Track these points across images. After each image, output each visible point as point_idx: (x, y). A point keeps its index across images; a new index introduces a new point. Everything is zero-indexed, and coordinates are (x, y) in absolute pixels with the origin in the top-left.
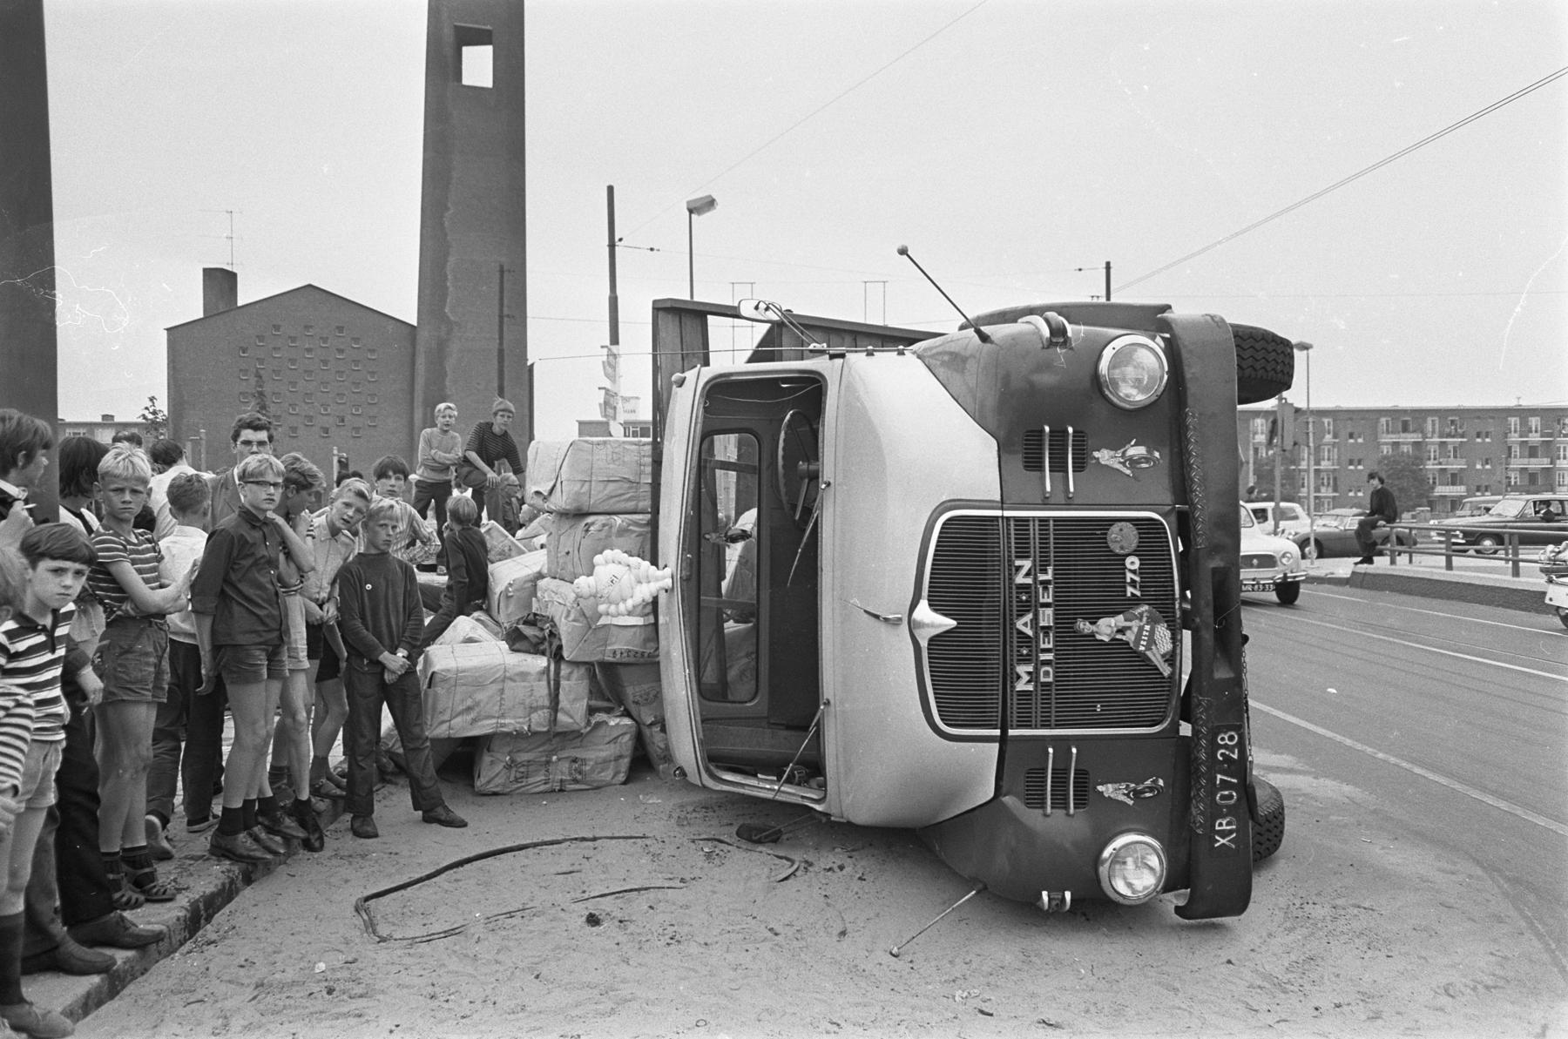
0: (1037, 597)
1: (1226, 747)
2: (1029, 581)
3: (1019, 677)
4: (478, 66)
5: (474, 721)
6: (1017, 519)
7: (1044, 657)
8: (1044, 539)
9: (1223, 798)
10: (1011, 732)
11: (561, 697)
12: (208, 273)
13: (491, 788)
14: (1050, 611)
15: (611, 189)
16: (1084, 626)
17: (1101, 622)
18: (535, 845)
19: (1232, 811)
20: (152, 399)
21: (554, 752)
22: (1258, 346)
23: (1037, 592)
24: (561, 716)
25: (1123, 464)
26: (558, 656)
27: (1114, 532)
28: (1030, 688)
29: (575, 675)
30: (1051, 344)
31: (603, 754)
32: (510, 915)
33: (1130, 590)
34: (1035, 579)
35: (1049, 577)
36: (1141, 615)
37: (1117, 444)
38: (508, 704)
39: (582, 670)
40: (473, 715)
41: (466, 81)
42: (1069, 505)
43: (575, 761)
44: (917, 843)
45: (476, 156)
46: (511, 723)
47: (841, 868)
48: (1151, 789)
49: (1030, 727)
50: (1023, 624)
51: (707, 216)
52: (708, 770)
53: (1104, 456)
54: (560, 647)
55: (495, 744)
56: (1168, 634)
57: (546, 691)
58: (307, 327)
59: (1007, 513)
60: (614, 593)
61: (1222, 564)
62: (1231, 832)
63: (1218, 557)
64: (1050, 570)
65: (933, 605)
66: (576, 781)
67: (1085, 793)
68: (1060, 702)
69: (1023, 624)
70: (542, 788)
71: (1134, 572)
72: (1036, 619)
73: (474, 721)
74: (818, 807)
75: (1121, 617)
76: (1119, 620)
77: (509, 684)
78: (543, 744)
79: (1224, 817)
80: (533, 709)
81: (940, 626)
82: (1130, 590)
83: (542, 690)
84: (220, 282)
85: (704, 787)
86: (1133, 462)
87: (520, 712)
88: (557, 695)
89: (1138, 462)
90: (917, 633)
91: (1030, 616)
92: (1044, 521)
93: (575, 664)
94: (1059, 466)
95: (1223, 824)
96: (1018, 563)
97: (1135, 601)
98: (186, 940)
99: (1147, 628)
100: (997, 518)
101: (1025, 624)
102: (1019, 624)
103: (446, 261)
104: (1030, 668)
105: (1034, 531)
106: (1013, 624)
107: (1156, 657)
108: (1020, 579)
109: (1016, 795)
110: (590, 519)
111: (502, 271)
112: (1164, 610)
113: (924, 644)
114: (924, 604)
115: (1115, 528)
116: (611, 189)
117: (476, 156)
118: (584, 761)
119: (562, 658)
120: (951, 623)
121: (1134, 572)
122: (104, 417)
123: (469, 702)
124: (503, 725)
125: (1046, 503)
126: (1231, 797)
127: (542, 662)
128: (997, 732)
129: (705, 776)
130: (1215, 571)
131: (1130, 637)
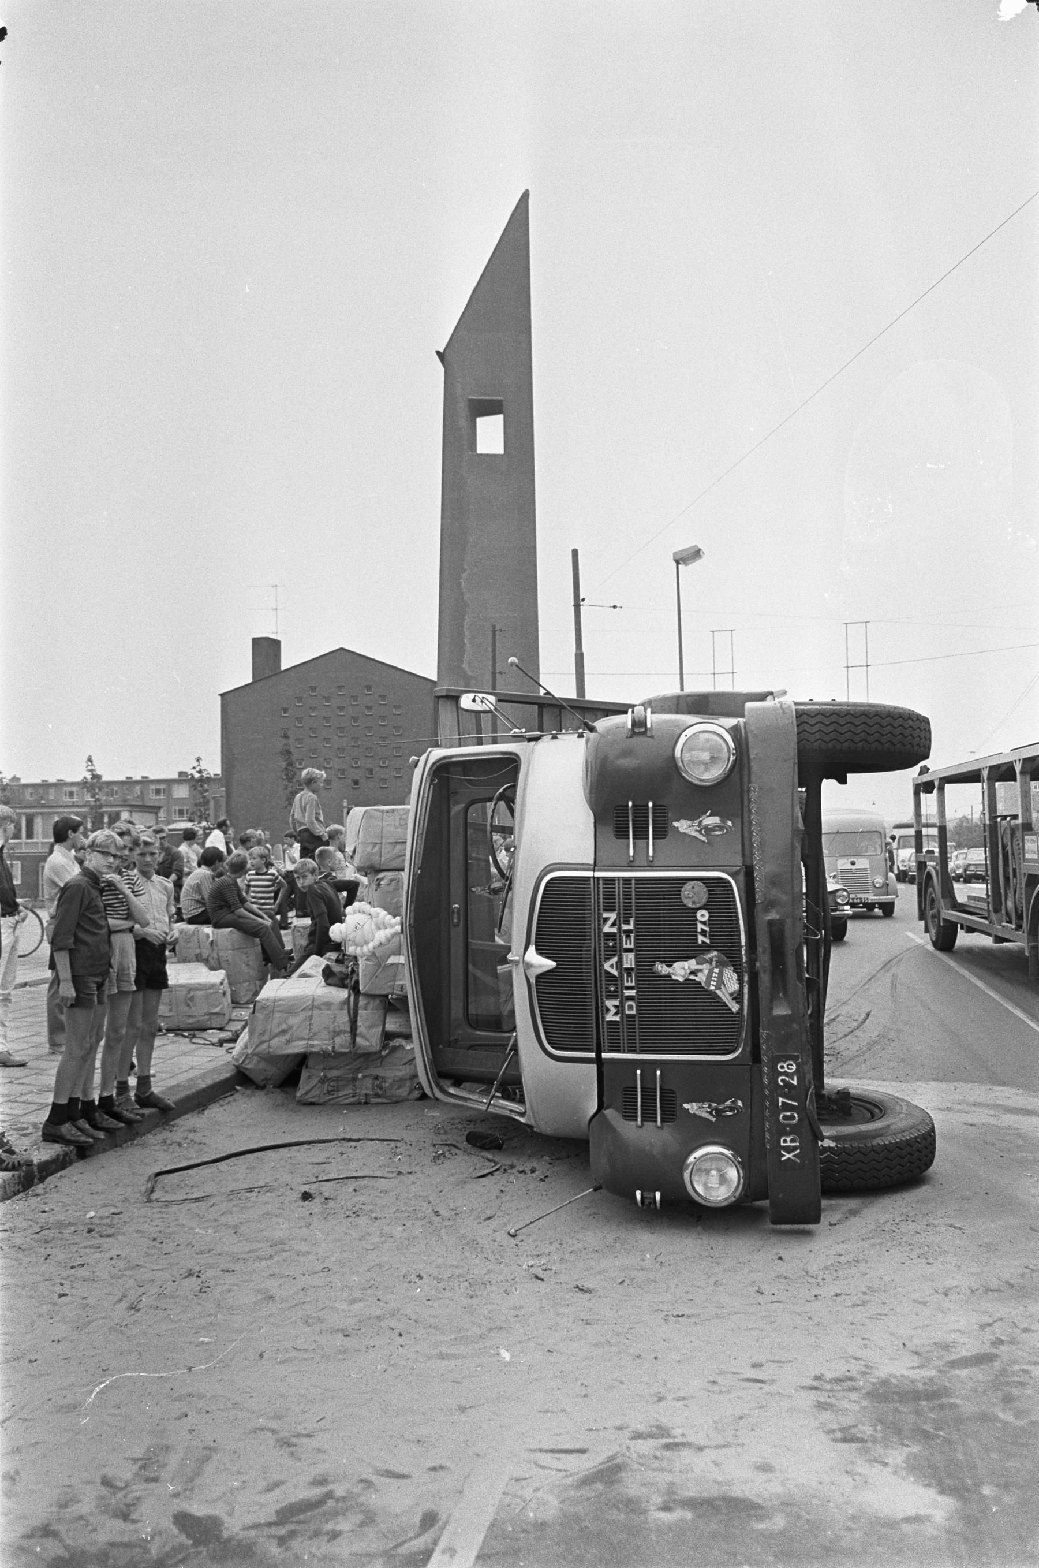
0: (621, 943)
1: (786, 1074)
2: (614, 930)
3: (608, 1010)
4: (490, 435)
5: (288, 1042)
6: (605, 879)
7: (627, 993)
8: (627, 895)
9: (785, 1118)
10: (604, 1055)
11: (359, 1023)
12: (256, 641)
13: (309, 1098)
14: (631, 955)
15: (575, 553)
16: (661, 968)
17: (676, 965)
18: (309, 1143)
19: (794, 1130)
20: (198, 760)
21: (359, 1070)
22: (896, 724)
23: (621, 940)
24: (358, 1040)
25: (700, 832)
26: (355, 989)
27: (687, 891)
28: (617, 1019)
29: (371, 1006)
30: (633, 733)
31: (400, 1074)
32: (251, 1190)
33: (701, 938)
34: (619, 928)
35: (631, 927)
36: (711, 960)
37: (692, 815)
38: (315, 1028)
39: (377, 1001)
40: (287, 1037)
41: (479, 451)
42: (651, 866)
43: (376, 1078)
44: (566, 1149)
45: (488, 521)
46: (319, 1044)
47: (533, 1171)
48: (731, 1109)
49: (618, 1051)
50: (610, 966)
51: (695, 565)
52: (438, 1085)
53: (682, 826)
54: (357, 982)
55: (311, 1062)
56: (735, 976)
57: (347, 1019)
58: (340, 687)
59: (597, 874)
60: (358, 936)
61: (778, 917)
62: (795, 1148)
63: (774, 911)
64: (632, 920)
65: (540, 951)
66: (377, 1096)
67: (671, 1112)
68: (642, 1031)
69: (610, 966)
70: (352, 1100)
71: (704, 923)
72: (620, 961)
73: (288, 1042)
74: (522, 1120)
75: (693, 961)
76: (692, 964)
77: (316, 1012)
78: (350, 1064)
79: (788, 1135)
80: (336, 1033)
81: (541, 966)
82: (701, 938)
83: (344, 1018)
84: (266, 649)
85: (437, 1099)
86: (708, 830)
87: (324, 1034)
88: (356, 1021)
89: (713, 830)
90: (528, 972)
91: (616, 959)
92: (627, 880)
93: (370, 996)
94: (641, 834)
95: (786, 1141)
96: (605, 915)
97: (706, 948)
98: (19, 1192)
99: (716, 970)
100: (587, 879)
101: (612, 966)
102: (607, 966)
103: (463, 619)
104: (617, 1003)
105: (619, 889)
106: (601, 966)
107: (724, 996)
108: (607, 929)
109: (617, 1109)
110: (381, 875)
111: (494, 632)
112: (730, 957)
113: (533, 981)
114: (532, 949)
115: (688, 886)
116: (575, 553)
117: (488, 521)
118: (384, 1079)
119: (359, 991)
120: (552, 964)
121: (704, 923)
122: (181, 773)
123: (284, 1026)
124: (313, 1046)
125: (631, 866)
126: (792, 1118)
127: (343, 994)
128: (593, 1055)
129: (436, 1090)
130: (770, 923)
131: (701, 978)
